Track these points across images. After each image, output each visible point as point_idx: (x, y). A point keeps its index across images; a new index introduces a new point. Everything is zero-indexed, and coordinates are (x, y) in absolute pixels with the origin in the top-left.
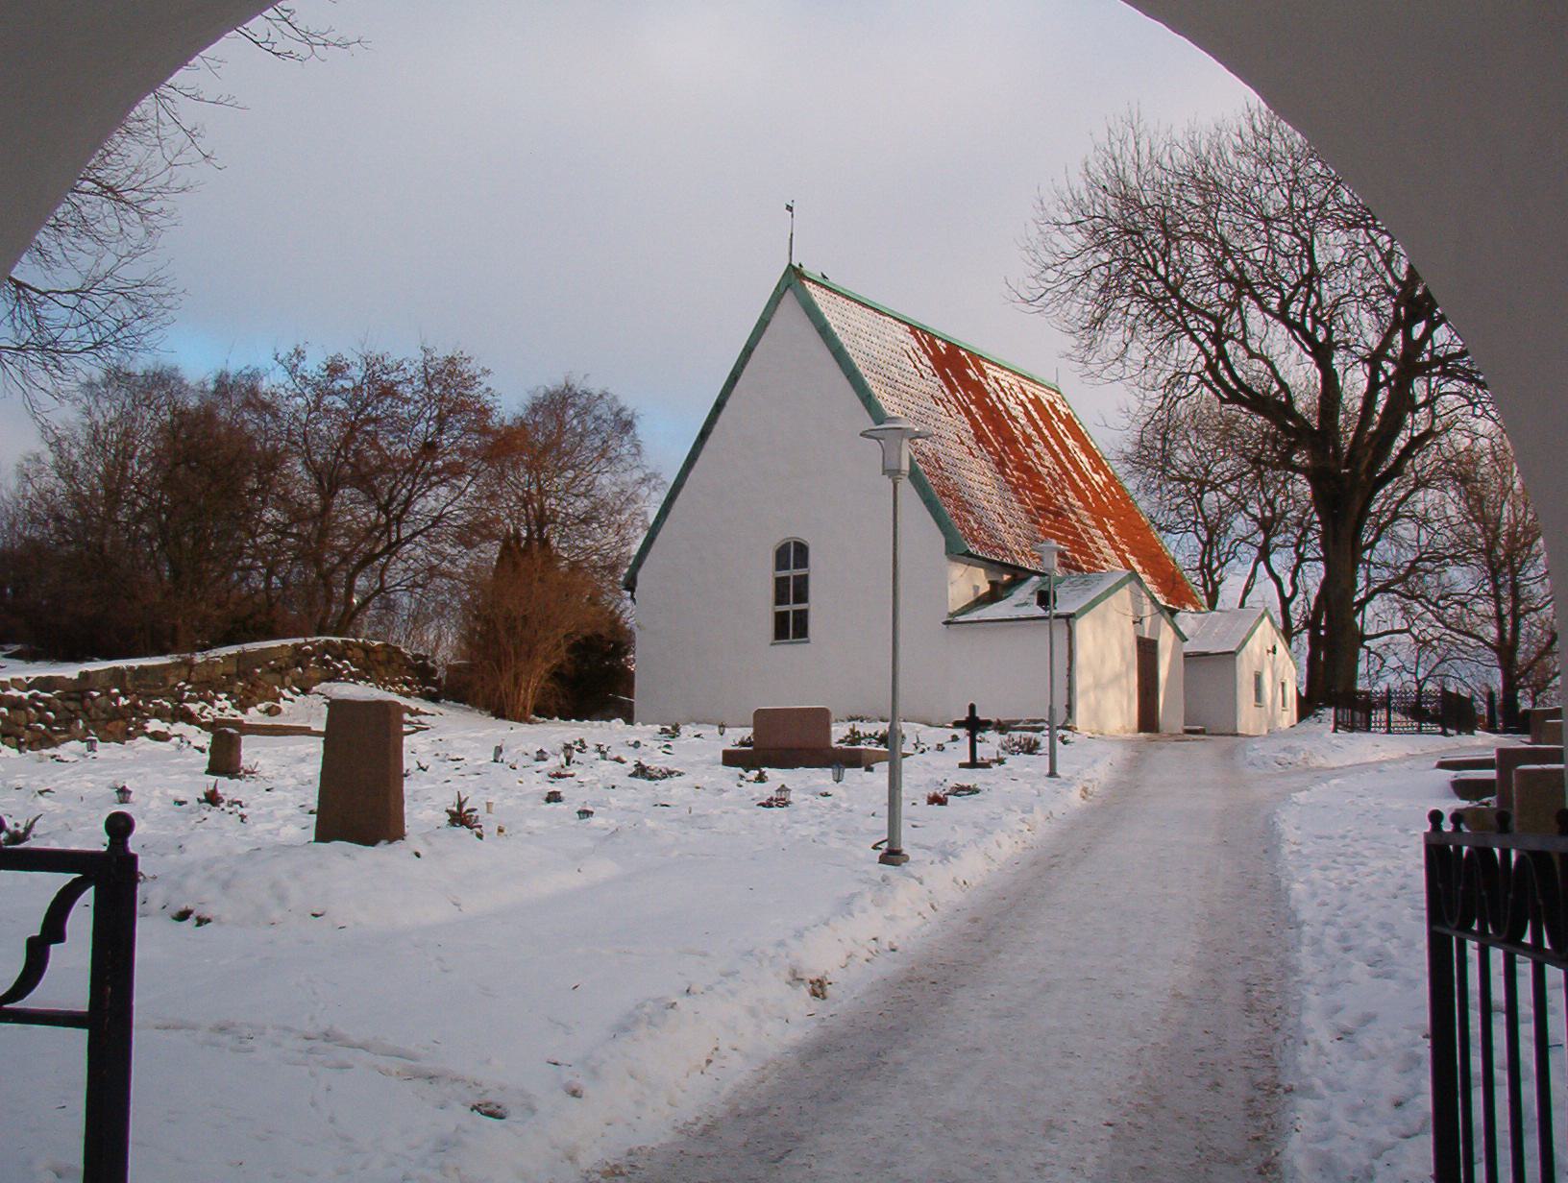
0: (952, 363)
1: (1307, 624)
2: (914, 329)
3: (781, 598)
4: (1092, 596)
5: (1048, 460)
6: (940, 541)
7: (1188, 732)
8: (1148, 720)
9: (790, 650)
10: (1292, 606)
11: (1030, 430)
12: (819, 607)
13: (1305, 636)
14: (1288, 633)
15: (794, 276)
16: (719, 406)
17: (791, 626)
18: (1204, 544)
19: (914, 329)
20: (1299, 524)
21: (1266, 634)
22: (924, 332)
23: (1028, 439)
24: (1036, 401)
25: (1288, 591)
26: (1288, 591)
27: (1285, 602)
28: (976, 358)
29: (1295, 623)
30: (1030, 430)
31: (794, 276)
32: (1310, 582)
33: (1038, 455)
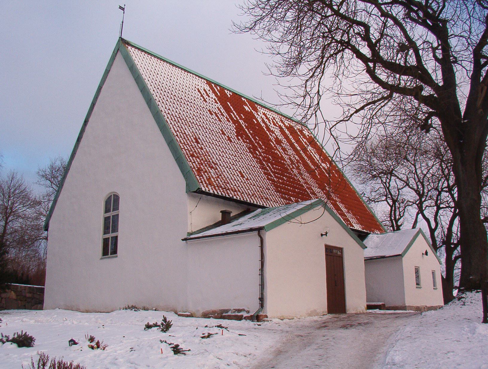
0: (232, 102)
1: (444, 243)
2: (209, 83)
3: (106, 230)
4: (289, 212)
5: (291, 152)
6: (182, 182)
7: (369, 307)
8: (336, 301)
9: (110, 262)
10: (436, 233)
11: (281, 137)
12: (124, 234)
13: (443, 248)
14: (435, 247)
15: (123, 42)
16: (86, 122)
17: (110, 248)
18: (391, 207)
19: (209, 83)
20: (436, 189)
21: (422, 244)
22: (216, 85)
23: (279, 142)
24: (290, 128)
25: (433, 225)
26: (433, 225)
27: (432, 231)
28: (253, 104)
29: (438, 243)
30: (281, 137)
31: (123, 42)
32: (443, 223)
33: (284, 150)
